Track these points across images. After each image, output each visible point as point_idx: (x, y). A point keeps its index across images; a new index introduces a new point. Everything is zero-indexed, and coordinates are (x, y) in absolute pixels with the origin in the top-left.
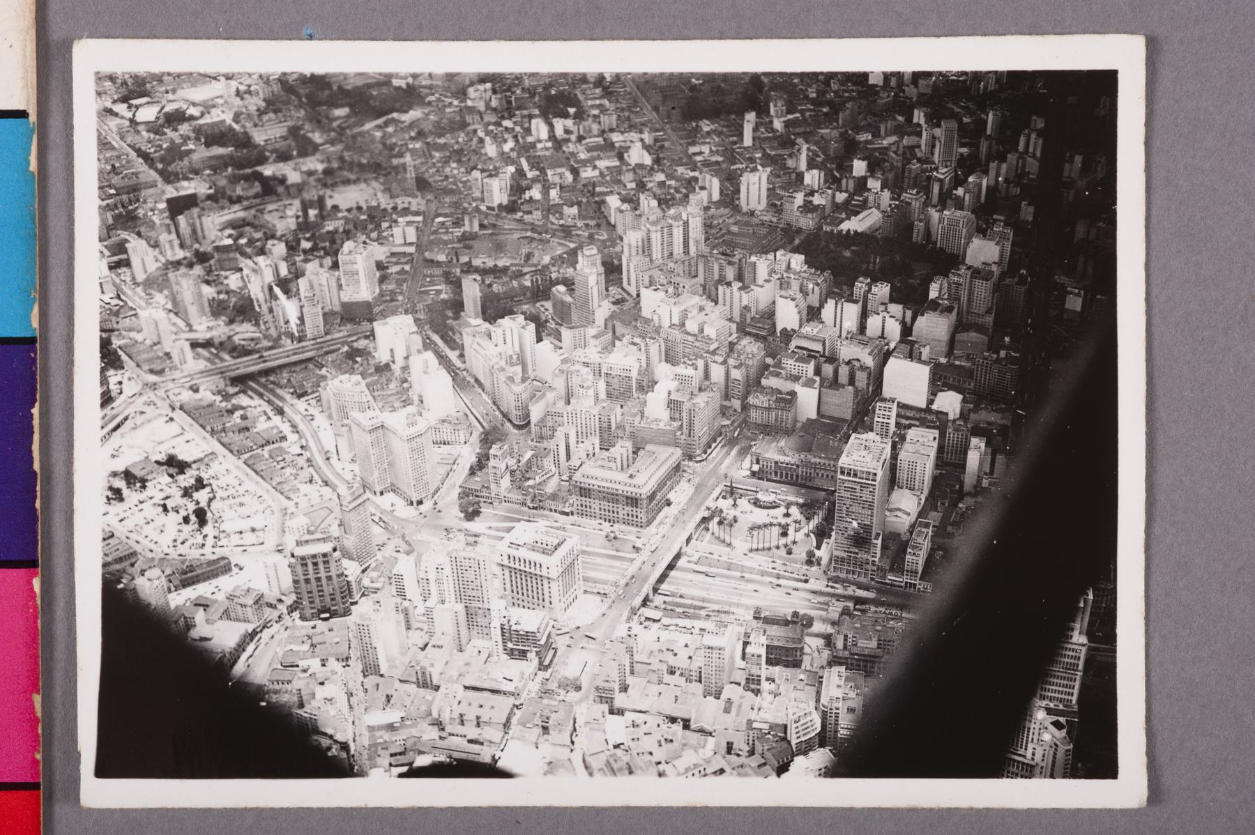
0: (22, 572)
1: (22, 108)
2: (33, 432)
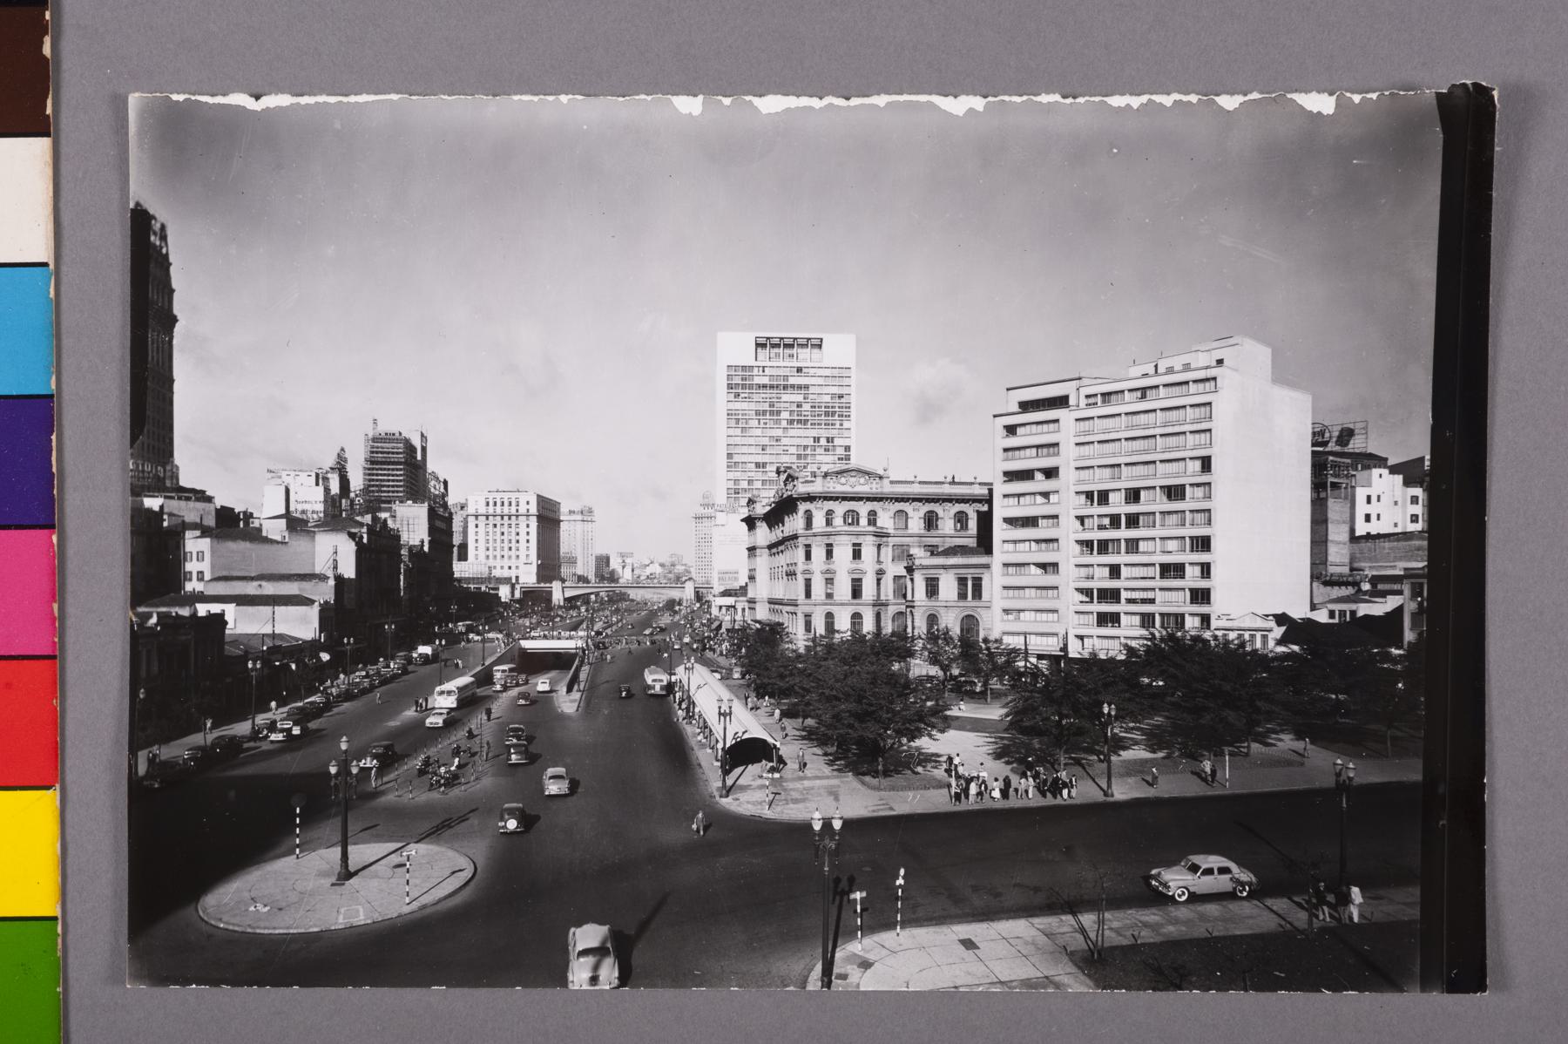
0: (46, 531)
1: (45, 261)
2: (52, 450)
